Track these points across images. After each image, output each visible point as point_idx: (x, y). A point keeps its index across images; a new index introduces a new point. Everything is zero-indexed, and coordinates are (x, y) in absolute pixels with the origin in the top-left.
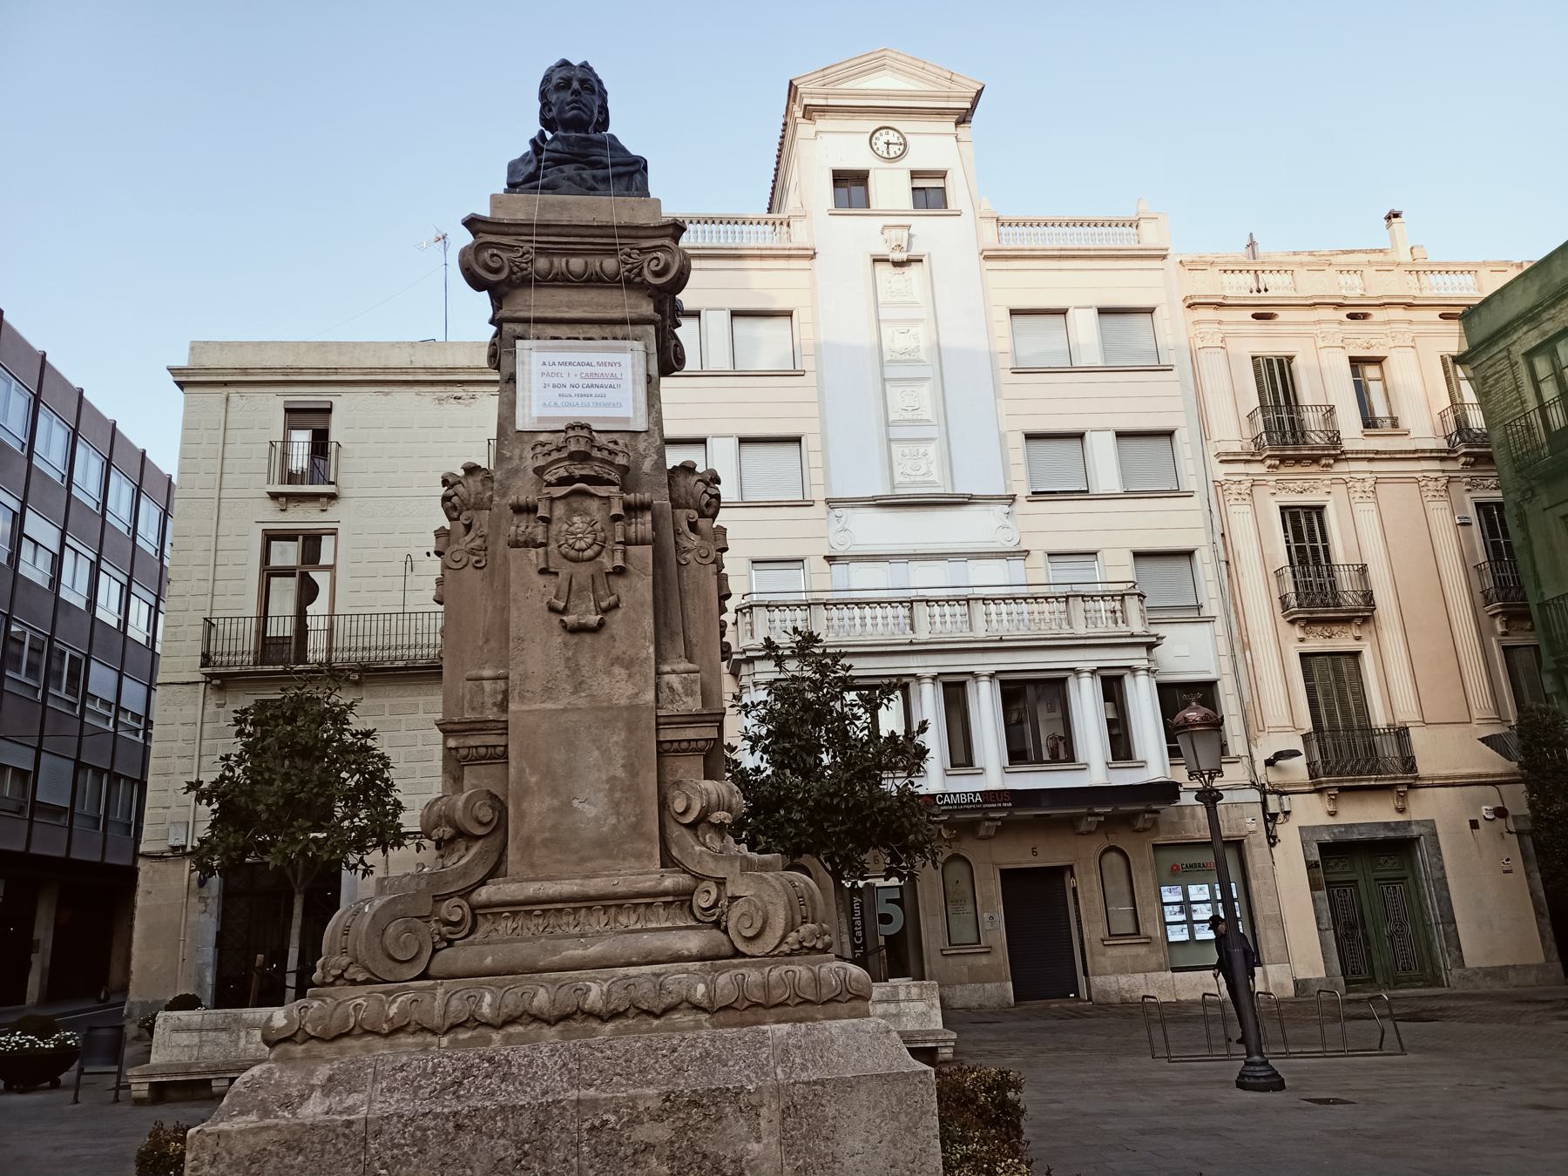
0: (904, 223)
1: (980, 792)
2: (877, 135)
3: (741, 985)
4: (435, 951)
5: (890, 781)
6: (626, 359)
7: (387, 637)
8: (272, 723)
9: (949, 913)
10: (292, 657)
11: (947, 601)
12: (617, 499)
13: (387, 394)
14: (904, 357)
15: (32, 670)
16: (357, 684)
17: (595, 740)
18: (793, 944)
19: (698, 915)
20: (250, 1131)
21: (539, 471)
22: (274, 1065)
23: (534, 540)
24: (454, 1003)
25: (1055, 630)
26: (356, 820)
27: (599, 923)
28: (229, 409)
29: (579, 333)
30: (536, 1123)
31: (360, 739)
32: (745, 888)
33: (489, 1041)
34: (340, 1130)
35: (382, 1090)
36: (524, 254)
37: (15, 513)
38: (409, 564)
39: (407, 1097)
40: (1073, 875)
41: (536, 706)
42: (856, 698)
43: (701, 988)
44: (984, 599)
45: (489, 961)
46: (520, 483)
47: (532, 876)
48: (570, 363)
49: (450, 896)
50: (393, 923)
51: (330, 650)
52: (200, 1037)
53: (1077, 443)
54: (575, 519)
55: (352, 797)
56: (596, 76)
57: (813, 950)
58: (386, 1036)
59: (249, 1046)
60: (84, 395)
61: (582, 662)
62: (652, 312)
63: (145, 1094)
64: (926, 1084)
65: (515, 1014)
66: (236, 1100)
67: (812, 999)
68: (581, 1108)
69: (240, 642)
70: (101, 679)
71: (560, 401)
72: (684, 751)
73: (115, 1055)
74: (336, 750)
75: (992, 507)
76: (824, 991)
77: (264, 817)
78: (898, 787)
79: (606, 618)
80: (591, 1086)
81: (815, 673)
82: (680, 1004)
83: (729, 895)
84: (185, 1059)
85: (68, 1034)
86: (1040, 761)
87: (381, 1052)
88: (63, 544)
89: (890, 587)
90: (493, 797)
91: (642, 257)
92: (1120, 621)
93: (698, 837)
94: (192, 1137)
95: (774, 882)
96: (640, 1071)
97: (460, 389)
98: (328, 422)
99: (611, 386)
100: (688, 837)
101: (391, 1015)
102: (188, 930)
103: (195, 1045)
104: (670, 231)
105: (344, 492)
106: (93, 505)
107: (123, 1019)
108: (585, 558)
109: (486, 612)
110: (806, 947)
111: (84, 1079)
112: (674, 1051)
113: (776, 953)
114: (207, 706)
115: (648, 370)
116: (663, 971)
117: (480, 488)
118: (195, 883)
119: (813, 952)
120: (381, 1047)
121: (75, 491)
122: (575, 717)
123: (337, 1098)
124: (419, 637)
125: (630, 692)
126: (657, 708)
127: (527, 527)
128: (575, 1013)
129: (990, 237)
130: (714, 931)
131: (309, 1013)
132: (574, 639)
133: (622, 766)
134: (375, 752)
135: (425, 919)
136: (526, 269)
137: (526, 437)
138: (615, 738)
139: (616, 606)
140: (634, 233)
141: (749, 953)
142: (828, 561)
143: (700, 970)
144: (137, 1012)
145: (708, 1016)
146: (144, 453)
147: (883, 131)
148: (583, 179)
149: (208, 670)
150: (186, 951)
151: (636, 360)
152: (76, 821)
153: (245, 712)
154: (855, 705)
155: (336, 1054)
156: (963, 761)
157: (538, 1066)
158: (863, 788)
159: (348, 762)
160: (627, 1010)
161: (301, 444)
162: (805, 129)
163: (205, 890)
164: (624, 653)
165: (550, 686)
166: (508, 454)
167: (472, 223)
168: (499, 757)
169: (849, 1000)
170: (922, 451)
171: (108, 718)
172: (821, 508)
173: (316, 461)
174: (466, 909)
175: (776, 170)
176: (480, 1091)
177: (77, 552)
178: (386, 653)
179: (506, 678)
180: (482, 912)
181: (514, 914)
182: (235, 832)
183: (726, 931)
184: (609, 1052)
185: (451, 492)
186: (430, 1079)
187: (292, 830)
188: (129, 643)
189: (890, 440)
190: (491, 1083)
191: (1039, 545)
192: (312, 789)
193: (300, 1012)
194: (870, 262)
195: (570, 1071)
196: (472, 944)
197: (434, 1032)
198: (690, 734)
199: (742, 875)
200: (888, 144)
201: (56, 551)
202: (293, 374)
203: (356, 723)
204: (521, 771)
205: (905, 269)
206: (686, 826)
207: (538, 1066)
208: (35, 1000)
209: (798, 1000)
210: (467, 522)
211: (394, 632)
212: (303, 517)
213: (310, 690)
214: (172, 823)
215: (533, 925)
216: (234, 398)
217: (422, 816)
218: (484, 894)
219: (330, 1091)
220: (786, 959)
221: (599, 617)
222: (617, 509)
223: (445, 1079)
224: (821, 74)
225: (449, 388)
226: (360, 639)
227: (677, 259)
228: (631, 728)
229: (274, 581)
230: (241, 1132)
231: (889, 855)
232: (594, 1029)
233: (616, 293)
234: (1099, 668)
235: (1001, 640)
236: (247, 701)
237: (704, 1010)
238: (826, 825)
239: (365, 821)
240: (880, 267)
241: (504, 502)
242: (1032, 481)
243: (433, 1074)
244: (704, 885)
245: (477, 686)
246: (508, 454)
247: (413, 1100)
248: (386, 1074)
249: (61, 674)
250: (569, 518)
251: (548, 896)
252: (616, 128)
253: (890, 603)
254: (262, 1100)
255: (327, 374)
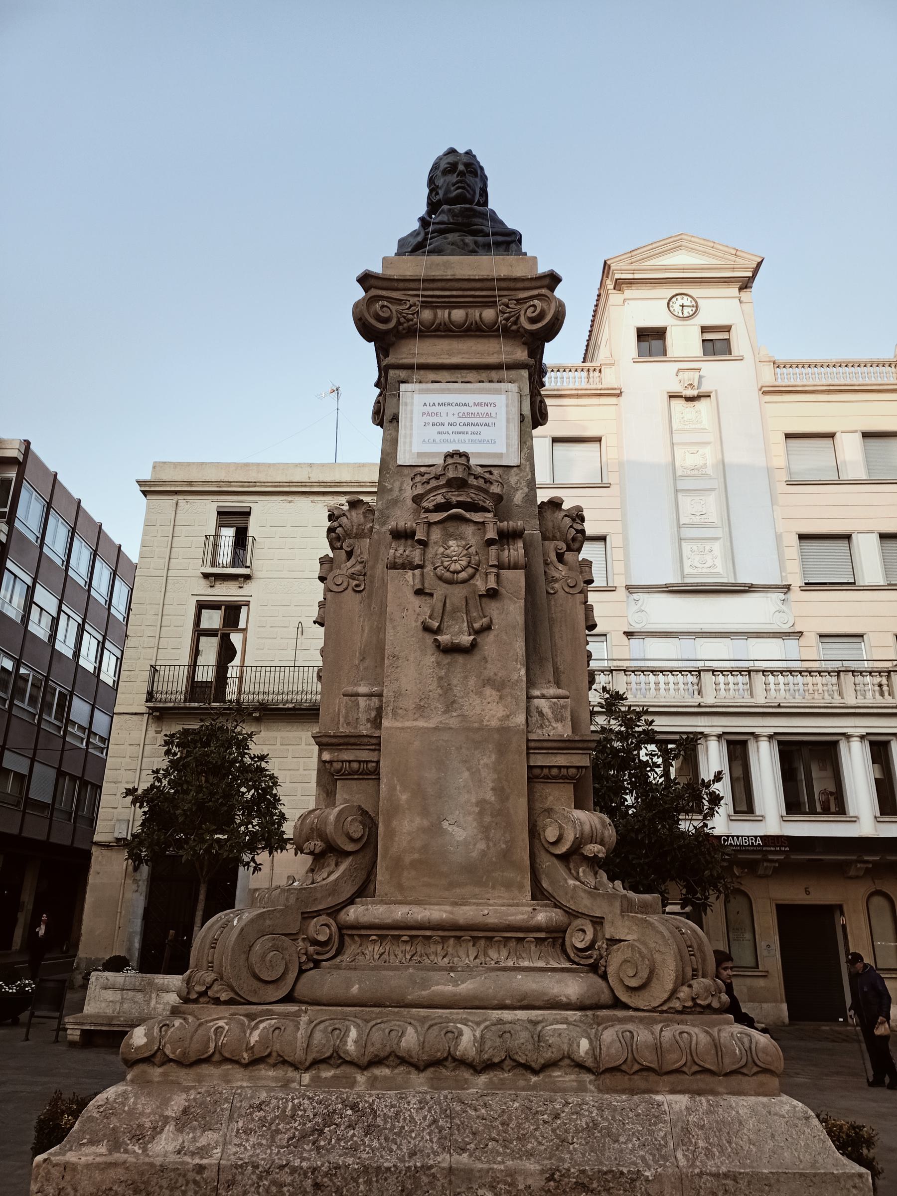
0: (696, 367)
1: (760, 836)
2: (674, 300)
3: (629, 1043)
4: (301, 972)
5: (688, 823)
6: (500, 400)
7: (281, 685)
8: (192, 745)
9: (731, 939)
10: (212, 697)
11: (731, 672)
12: (491, 524)
13: (290, 501)
14: (693, 472)
15: (33, 700)
16: (258, 720)
17: (466, 761)
18: (685, 1001)
19: (572, 955)
20: (98, 1166)
21: (417, 499)
22: (130, 1088)
23: (411, 563)
24: (318, 1036)
25: (828, 699)
26: (250, 826)
27: (468, 956)
28: (178, 511)
30: (403, 1191)
31: (256, 762)
32: (626, 931)
33: (353, 1084)
34: (191, 1175)
35: (238, 1130)
36: (411, 306)
37: (28, 586)
38: (300, 629)
39: (264, 1142)
40: (842, 914)
41: (408, 724)
42: (656, 749)
43: (584, 1044)
44: (764, 671)
45: (355, 989)
46: (399, 513)
47: (400, 898)
49: (318, 913)
50: (261, 940)
51: (239, 693)
52: (122, 995)
53: (845, 543)
54: (451, 543)
55: (249, 808)
56: (478, 163)
57: (708, 1009)
58: (246, 1066)
59: (158, 1006)
60: (82, 504)
61: (455, 682)
62: (527, 357)
63: (77, 1038)
64: (861, 1190)
65: (382, 1054)
66: (88, 1125)
67: (712, 1068)
68: (453, 1178)
69: (175, 684)
70: (79, 709)
72: (555, 777)
73: (58, 1004)
74: (238, 770)
75: (769, 595)
76: (727, 1061)
77: (181, 819)
78: (695, 827)
79: (479, 640)
80: (464, 1150)
81: (621, 726)
82: (561, 1060)
83: (608, 936)
84: (109, 1012)
85: (27, 982)
86: (813, 812)
87: (239, 1084)
88: (60, 610)
89: (680, 658)
90: (364, 813)
92: (886, 694)
93: (570, 870)
94: (38, 1166)
95: (662, 929)
96: (518, 1139)
98: (247, 522)
99: (486, 425)
100: (560, 869)
101: (252, 1042)
102: (124, 905)
103: (118, 1002)
105: (256, 574)
106: (82, 583)
107: (73, 971)
108: (459, 580)
109: (363, 631)
110: (700, 1005)
111: (34, 1020)
112: (557, 1117)
113: (665, 1008)
114: (148, 732)
115: (521, 410)
116: (540, 1018)
117: (362, 520)
118: (131, 868)
119: (708, 1011)
120: (241, 1080)
121: (71, 573)
122: (446, 736)
123: (191, 1135)
124: (305, 685)
125: (501, 714)
126: (528, 732)
127: (405, 551)
128: (446, 1059)
129: (768, 376)
130: (591, 975)
131: (169, 1033)
132: (447, 659)
133: (492, 789)
134: (267, 773)
135: (293, 937)
136: (412, 320)
138: (485, 760)
139: (488, 628)
141: (632, 1005)
142: (627, 636)
143: (581, 1021)
144: (83, 966)
145: (592, 1077)
146: (120, 547)
147: (679, 297)
148: (466, 244)
149: (150, 704)
150: (122, 921)
151: (510, 402)
152: (55, 814)
153: (172, 736)
154: (654, 755)
155: (194, 1081)
156: (745, 808)
157: (405, 1119)
158: (663, 827)
159: (246, 779)
160: (502, 1061)
161: (227, 538)
162: (615, 298)
163: (138, 874)
164: (496, 674)
165: (422, 704)
166: (389, 487)
167: (366, 280)
168: (371, 773)
169: (755, 1074)
170: (708, 548)
171: (83, 739)
172: (622, 593)
173: (238, 551)
174: (334, 928)
175: (590, 331)
176: (342, 1143)
177: (69, 616)
178: (280, 697)
179: (381, 695)
180: (350, 933)
181: (382, 938)
182: (159, 830)
183: (604, 977)
184: (483, 1111)
185: (336, 524)
186: (288, 1123)
187: (201, 831)
188: (100, 684)
189: (681, 539)
190: (354, 1135)
191: (812, 627)
192: (218, 799)
193: (160, 1031)
194: (666, 397)
195: (441, 1129)
196: (338, 967)
197: (295, 1067)
198: (561, 760)
199: (623, 916)
200: (683, 306)
201: (55, 615)
202: (223, 486)
203: (255, 748)
204: (392, 789)
205: (696, 403)
206: (558, 856)
207: (405, 1119)
208: (18, 948)
209: (696, 1068)
210: (349, 549)
211: (286, 681)
212: (226, 592)
213: (221, 722)
214: (118, 820)
215: (400, 953)
216: (182, 503)
217: (295, 827)
218: (353, 913)
219: (184, 1126)
220: (678, 1017)
221: (472, 637)
222: (491, 534)
223: (305, 1124)
224: (630, 255)
225: (336, 498)
226: (262, 685)
228: (502, 750)
229: (203, 639)
230: (88, 1166)
231: (685, 887)
232: (466, 1080)
234: (868, 734)
235: (779, 706)
236: (176, 728)
237: (589, 1070)
238: (631, 857)
239: (257, 828)
240: (674, 402)
241: (384, 529)
242: (804, 573)
243: (293, 1117)
244: (578, 922)
245: (352, 702)
246: (389, 487)
247: (270, 1147)
248: (243, 1112)
249: (52, 705)
250: (445, 541)
251: (417, 921)
252: (493, 204)
253: (680, 672)
254: (113, 1129)
255: (248, 487)
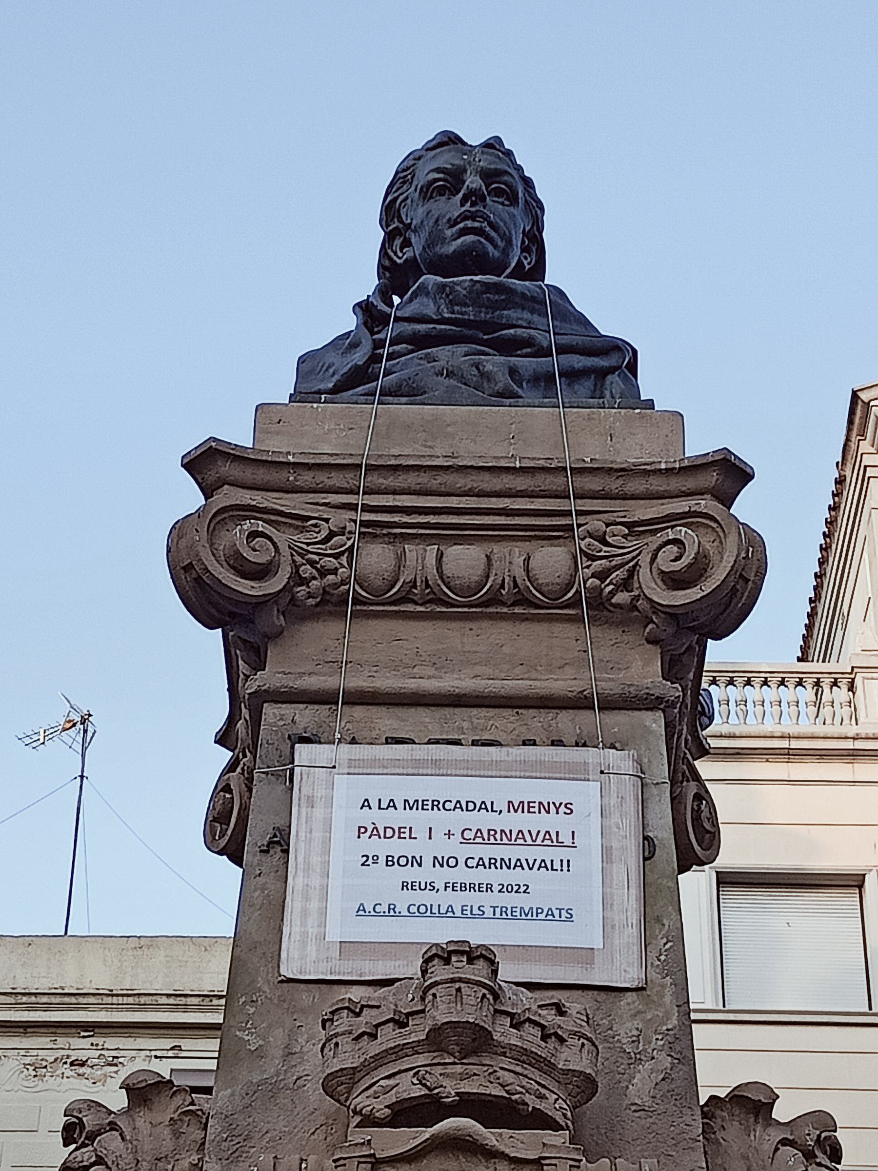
29: (461, 730)
36: (331, 535)
48: (435, 804)
56: (519, 169)
71: (403, 900)
91: (633, 543)
97: (85, 1043)
99: (543, 865)
104: (711, 478)
137: (305, 997)
140: (614, 485)
225: (61, 1041)
227: (731, 543)
233: (564, 632)
